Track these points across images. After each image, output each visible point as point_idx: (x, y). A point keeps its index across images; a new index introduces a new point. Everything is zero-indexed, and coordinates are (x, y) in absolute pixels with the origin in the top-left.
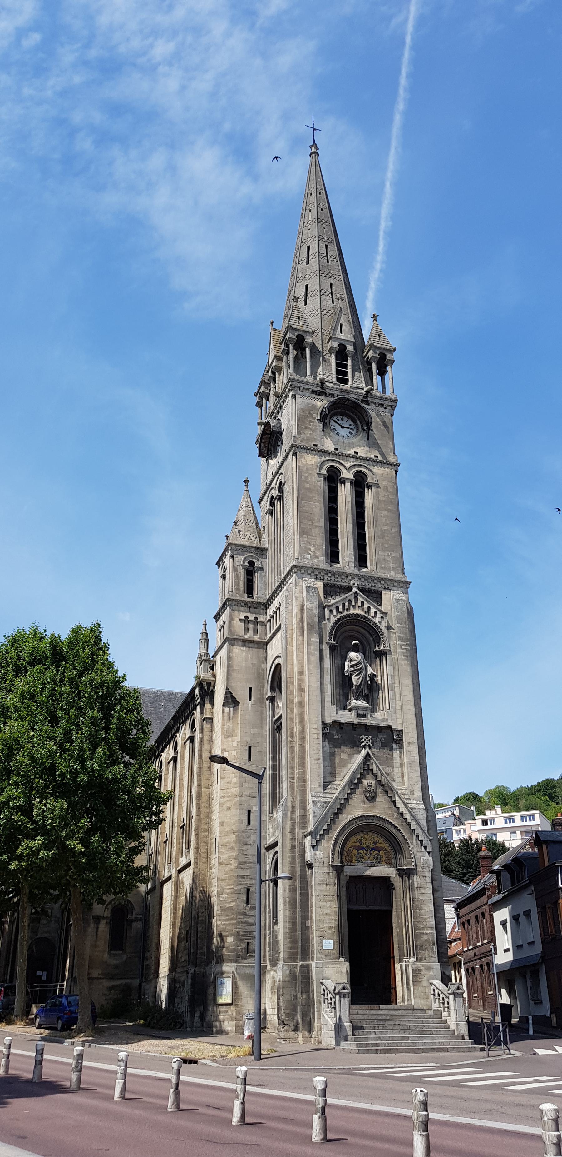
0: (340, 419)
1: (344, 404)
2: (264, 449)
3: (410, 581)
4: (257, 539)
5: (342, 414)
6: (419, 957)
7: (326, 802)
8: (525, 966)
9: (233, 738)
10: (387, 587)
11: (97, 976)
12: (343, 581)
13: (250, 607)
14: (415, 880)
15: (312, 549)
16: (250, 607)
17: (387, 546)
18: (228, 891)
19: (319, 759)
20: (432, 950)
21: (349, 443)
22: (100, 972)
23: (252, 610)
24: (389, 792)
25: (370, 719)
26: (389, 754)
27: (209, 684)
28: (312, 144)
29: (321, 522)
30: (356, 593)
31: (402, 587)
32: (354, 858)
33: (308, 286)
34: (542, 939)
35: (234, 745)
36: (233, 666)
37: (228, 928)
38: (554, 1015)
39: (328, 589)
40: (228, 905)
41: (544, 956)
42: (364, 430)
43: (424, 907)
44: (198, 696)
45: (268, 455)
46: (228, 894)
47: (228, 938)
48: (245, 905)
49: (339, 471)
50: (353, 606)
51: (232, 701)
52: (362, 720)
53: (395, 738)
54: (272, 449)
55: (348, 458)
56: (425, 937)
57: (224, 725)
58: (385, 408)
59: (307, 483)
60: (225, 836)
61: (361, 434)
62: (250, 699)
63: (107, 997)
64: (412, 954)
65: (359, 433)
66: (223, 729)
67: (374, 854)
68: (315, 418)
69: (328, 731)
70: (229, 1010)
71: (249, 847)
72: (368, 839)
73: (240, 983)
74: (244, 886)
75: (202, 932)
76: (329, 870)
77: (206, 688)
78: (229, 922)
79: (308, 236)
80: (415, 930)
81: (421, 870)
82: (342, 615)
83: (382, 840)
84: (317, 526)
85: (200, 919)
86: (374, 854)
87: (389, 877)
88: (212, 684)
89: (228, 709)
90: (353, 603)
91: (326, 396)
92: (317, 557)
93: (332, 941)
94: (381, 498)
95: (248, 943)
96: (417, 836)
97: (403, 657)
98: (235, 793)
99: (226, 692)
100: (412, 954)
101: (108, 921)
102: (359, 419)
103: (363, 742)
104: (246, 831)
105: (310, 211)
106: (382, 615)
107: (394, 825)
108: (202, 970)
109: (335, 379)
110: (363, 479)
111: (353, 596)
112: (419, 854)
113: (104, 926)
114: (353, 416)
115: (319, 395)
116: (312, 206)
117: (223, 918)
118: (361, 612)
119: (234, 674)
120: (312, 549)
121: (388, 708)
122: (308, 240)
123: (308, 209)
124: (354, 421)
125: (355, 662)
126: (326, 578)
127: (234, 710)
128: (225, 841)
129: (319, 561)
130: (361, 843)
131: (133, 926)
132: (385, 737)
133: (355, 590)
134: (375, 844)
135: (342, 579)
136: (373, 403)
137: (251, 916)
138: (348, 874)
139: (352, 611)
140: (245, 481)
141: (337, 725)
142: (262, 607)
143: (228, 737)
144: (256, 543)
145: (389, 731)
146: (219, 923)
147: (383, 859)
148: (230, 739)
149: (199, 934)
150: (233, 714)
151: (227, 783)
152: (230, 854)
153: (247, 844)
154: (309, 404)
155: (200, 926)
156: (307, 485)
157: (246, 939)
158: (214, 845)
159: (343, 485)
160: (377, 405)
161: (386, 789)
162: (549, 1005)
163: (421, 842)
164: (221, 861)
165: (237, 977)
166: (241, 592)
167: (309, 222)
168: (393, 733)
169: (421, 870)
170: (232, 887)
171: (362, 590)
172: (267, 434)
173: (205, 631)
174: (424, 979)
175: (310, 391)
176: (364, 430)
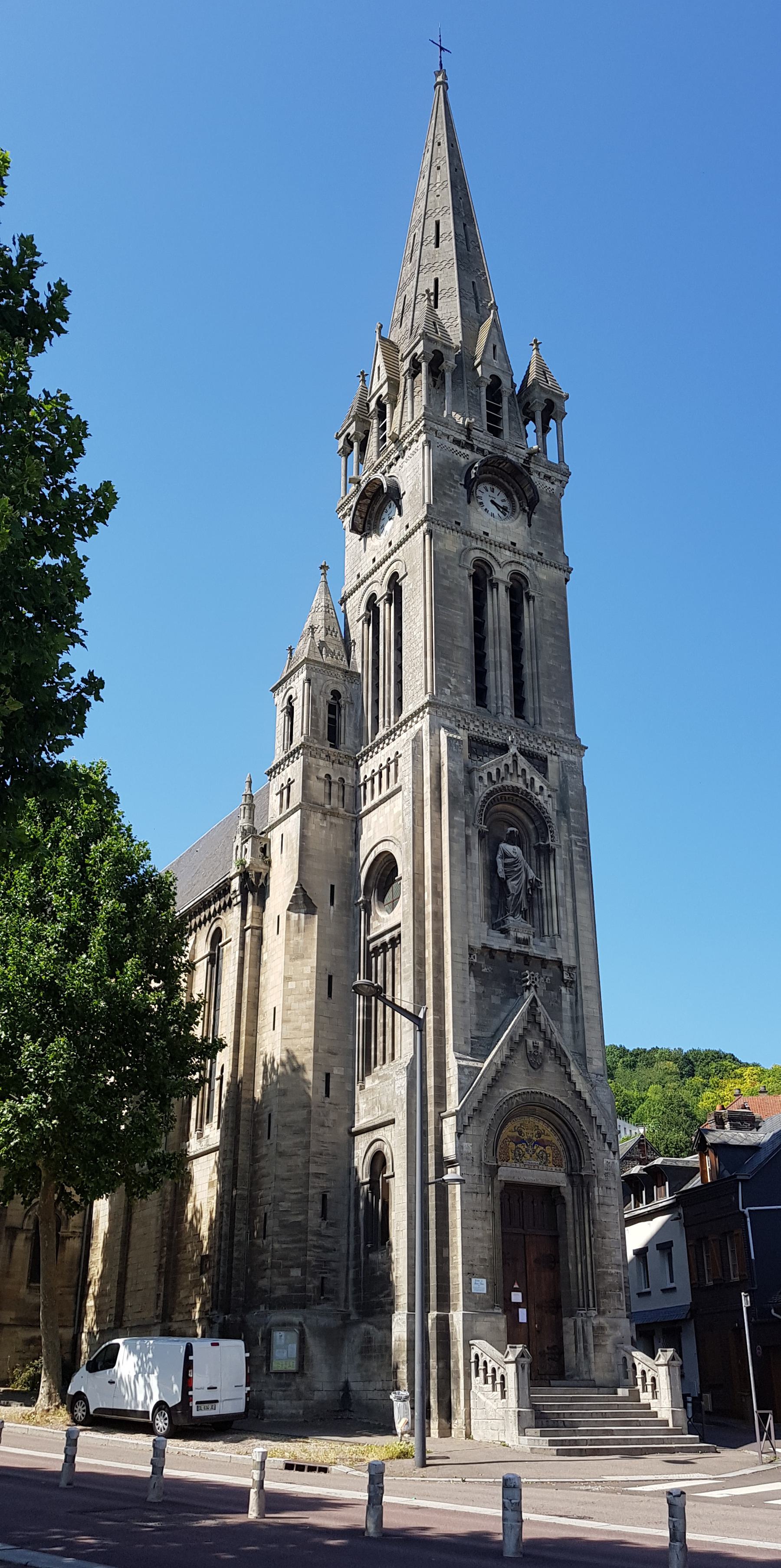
0: (489, 489)
1: (497, 467)
2: (359, 521)
3: (586, 745)
4: (345, 659)
5: (493, 482)
6: (602, 1308)
7: (476, 1068)
8: (655, 1323)
9: (305, 960)
10: (554, 751)
11: (8, 1321)
12: (495, 735)
13: (333, 762)
14: (596, 1194)
15: (453, 680)
16: (333, 762)
17: (554, 690)
18: (293, 1197)
19: (464, 1002)
20: (619, 1300)
21: (504, 528)
22: (13, 1316)
23: (336, 765)
24: (563, 1058)
25: (534, 947)
26: (556, 1002)
27: (258, 875)
28: (439, 69)
29: (466, 643)
30: (515, 755)
31: (574, 754)
32: (511, 1155)
33: (440, 281)
34: (692, 1285)
35: (305, 972)
36: (307, 850)
37: (293, 1255)
38: (709, 1395)
39: (474, 744)
40: (293, 1219)
41: (694, 1311)
42: (524, 510)
43: (608, 1234)
44: (238, 893)
45: (364, 531)
46: (292, 1201)
47: (291, 1270)
48: (319, 1220)
49: (490, 567)
50: (511, 774)
51: (304, 903)
52: (523, 948)
53: (565, 977)
54: (372, 522)
55: (502, 550)
56: (610, 1279)
57: (289, 940)
58: (553, 483)
59: (447, 578)
60: (288, 1111)
61: (520, 516)
62: (332, 903)
63: (23, 1356)
64: (591, 1304)
65: (516, 515)
66: (287, 945)
67: (538, 1151)
68: (457, 482)
69: (475, 960)
70: (293, 1383)
71: (327, 1130)
72: (531, 1126)
73: (310, 1341)
74: (319, 1190)
75: (237, 1259)
76: (481, 1171)
77: (254, 880)
78: (294, 1245)
79: (436, 205)
80: (596, 1268)
81: (603, 1177)
82: (495, 786)
83: (548, 1130)
84: (458, 647)
85: (236, 1239)
86: (538, 1151)
87: (559, 1187)
88: (264, 875)
89: (297, 915)
90: (511, 771)
91: (472, 450)
92: (459, 694)
93: (484, 1281)
94: (547, 618)
95: (323, 1278)
96: (599, 1127)
97: (578, 859)
98: (307, 1046)
99: (296, 889)
100: (591, 1304)
101: (29, 1235)
102: (517, 494)
103: (527, 981)
104: (323, 1105)
105: (439, 168)
106: (550, 793)
107: (568, 1108)
108: (239, 1319)
109: (485, 427)
110: (521, 584)
111: (511, 759)
112: (602, 1154)
113: (22, 1244)
114: (510, 488)
115: (463, 448)
116: (442, 163)
117: (283, 1239)
118: (520, 784)
119: (309, 862)
120: (453, 680)
121: (556, 932)
122: (437, 211)
123: (434, 165)
124: (509, 495)
125: (513, 860)
126: (472, 727)
127: (306, 918)
128: (288, 1119)
129: (462, 701)
130: (520, 1133)
131: (67, 1245)
132: (551, 975)
133: (513, 750)
134: (539, 1135)
135: (494, 731)
136: (537, 472)
137: (329, 1237)
138: (503, 1179)
139: (508, 782)
140: (322, 567)
141: (490, 952)
142: (351, 763)
143: (296, 958)
144: (343, 663)
145: (556, 967)
146: (276, 1246)
147: (550, 1159)
148: (299, 962)
149: (235, 1262)
150: (305, 923)
151: (294, 1029)
152: (298, 1140)
153: (323, 1126)
154: (449, 459)
155: (237, 1250)
156: (446, 583)
157: (321, 1273)
158: (266, 1125)
159: (495, 590)
160: (542, 477)
161: (559, 1053)
162: (698, 1379)
163: (605, 1135)
164: (280, 1150)
165: (307, 1330)
166: (321, 737)
167: (438, 185)
168: (562, 971)
169: (603, 1177)
170: (300, 1190)
171: (523, 752)
172: (367, 498)
173: (249, 792)
174: (609, 1343)
175: (451, 438)
176: (524, 510)
